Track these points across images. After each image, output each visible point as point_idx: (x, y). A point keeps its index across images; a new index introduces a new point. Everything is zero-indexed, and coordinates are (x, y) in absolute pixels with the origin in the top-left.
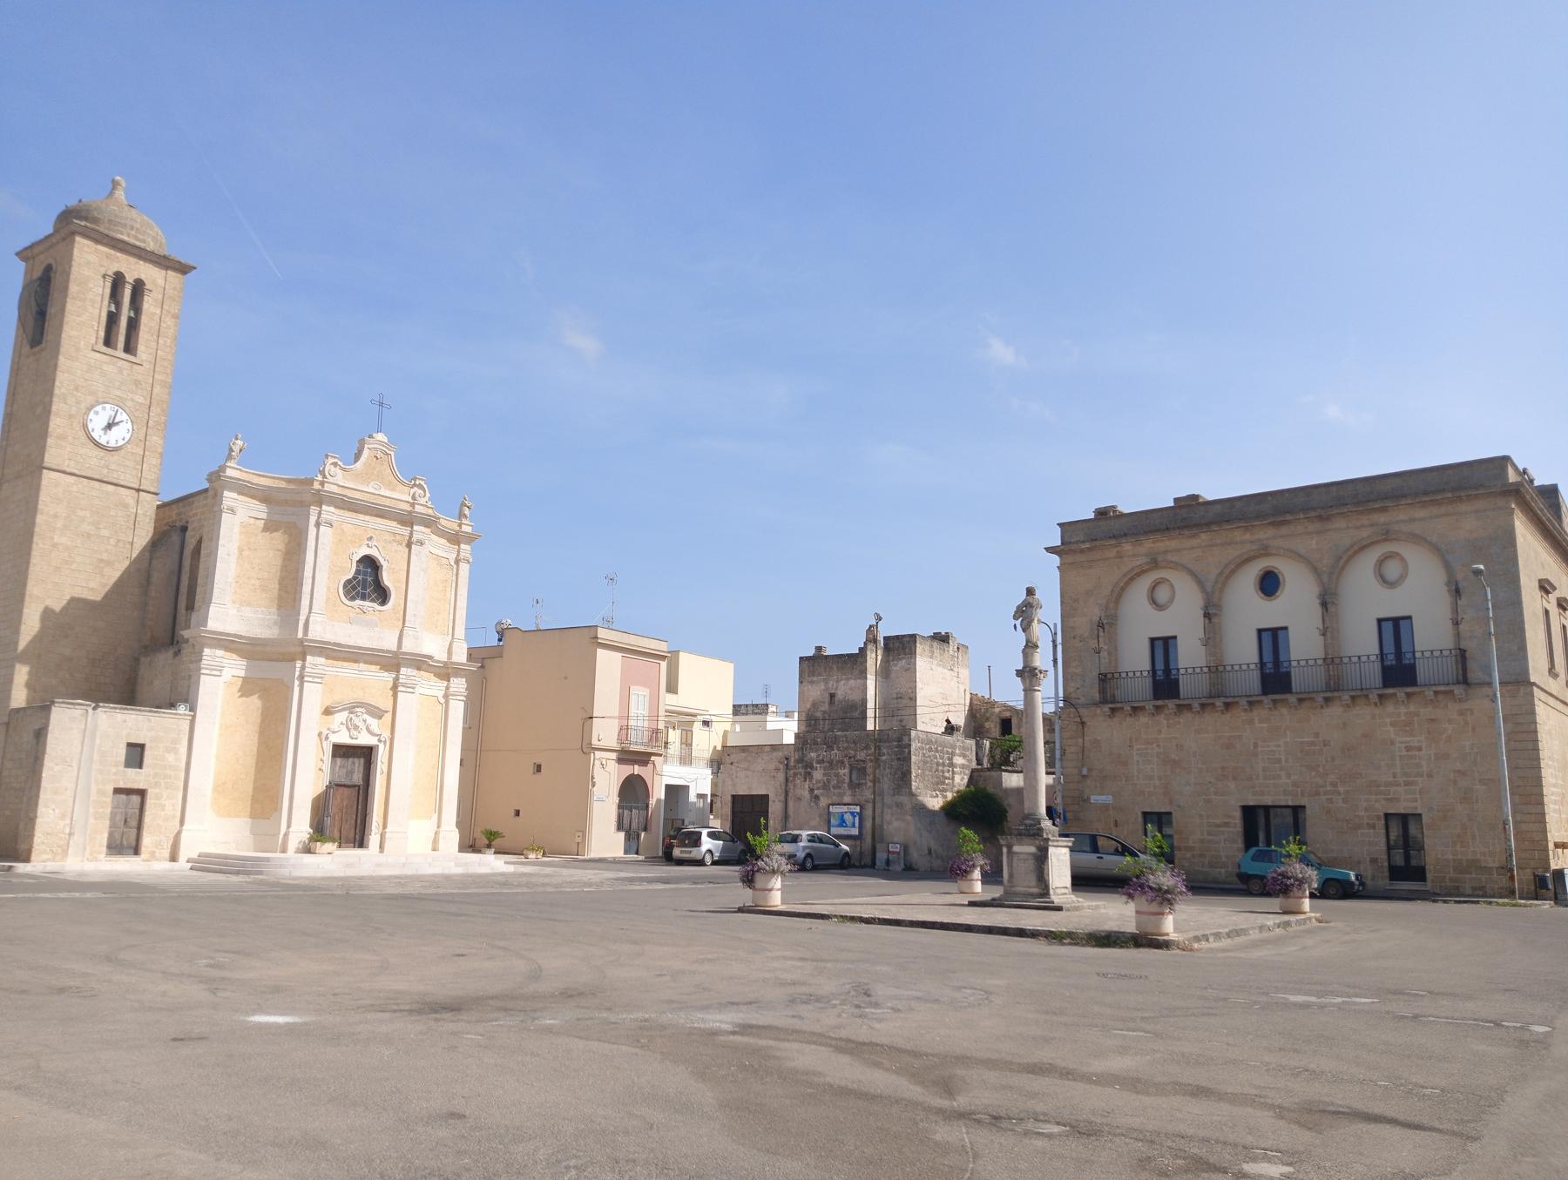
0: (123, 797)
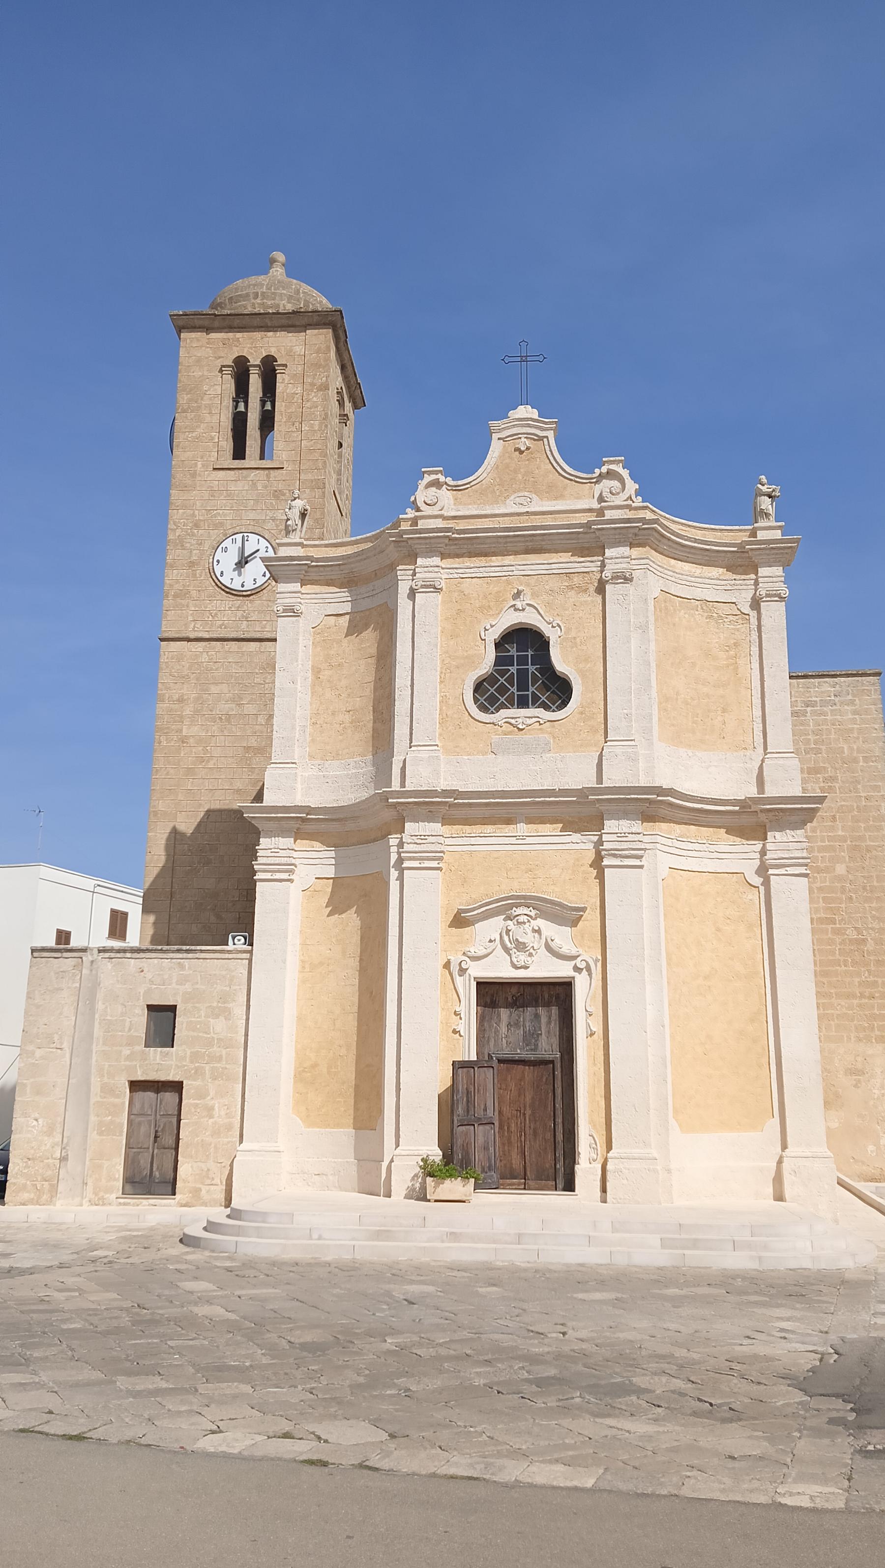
0: (151, 1095)
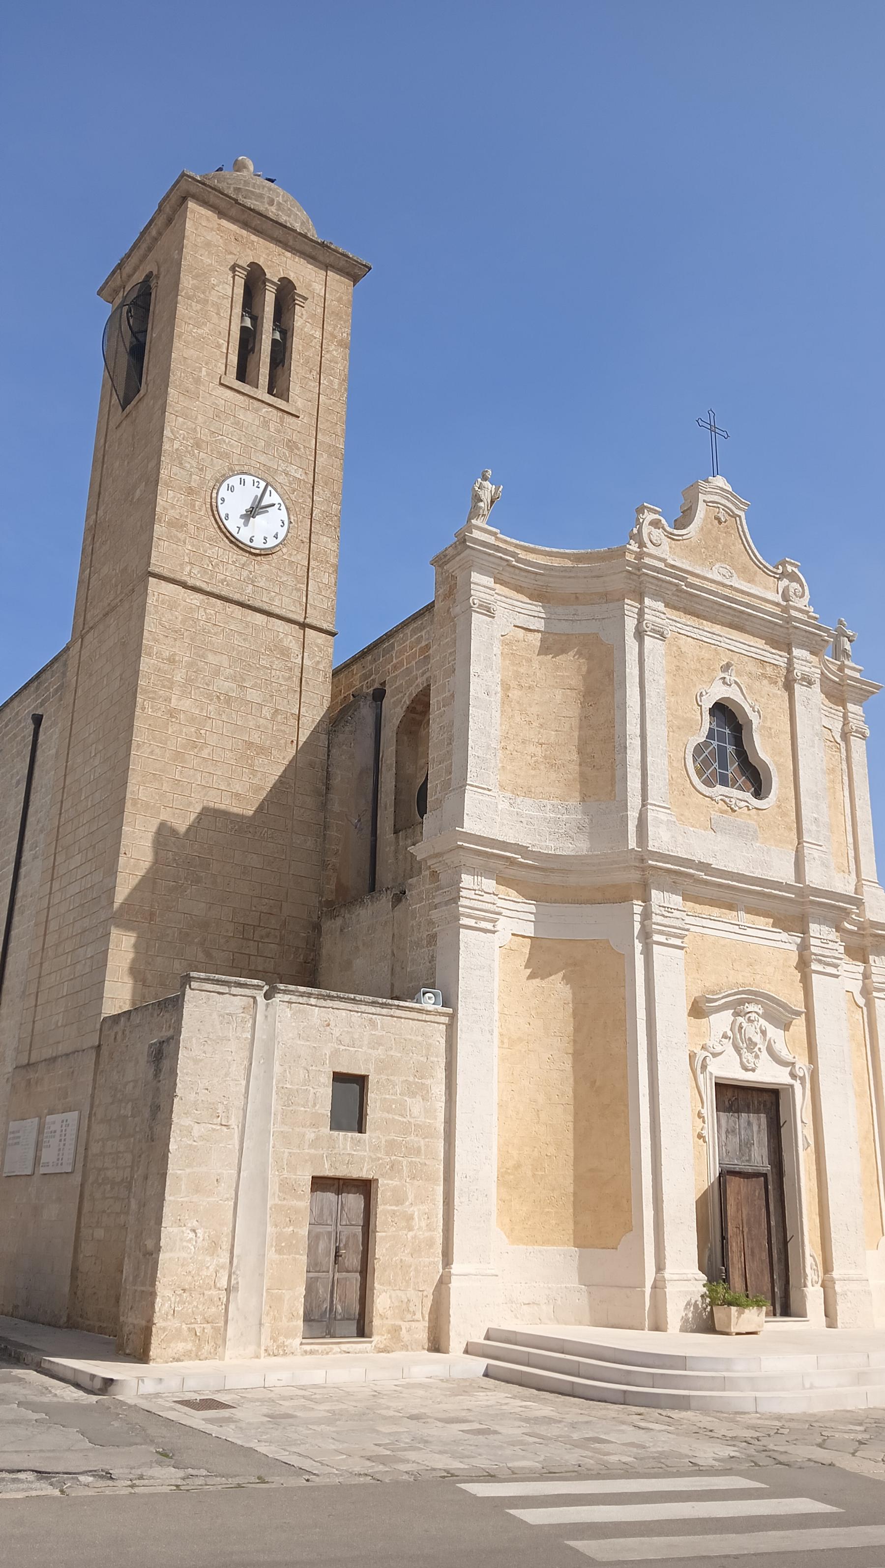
0: (331, 1196)
